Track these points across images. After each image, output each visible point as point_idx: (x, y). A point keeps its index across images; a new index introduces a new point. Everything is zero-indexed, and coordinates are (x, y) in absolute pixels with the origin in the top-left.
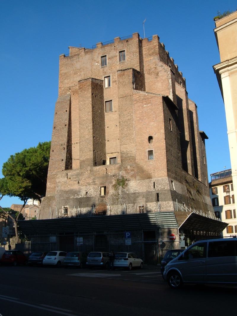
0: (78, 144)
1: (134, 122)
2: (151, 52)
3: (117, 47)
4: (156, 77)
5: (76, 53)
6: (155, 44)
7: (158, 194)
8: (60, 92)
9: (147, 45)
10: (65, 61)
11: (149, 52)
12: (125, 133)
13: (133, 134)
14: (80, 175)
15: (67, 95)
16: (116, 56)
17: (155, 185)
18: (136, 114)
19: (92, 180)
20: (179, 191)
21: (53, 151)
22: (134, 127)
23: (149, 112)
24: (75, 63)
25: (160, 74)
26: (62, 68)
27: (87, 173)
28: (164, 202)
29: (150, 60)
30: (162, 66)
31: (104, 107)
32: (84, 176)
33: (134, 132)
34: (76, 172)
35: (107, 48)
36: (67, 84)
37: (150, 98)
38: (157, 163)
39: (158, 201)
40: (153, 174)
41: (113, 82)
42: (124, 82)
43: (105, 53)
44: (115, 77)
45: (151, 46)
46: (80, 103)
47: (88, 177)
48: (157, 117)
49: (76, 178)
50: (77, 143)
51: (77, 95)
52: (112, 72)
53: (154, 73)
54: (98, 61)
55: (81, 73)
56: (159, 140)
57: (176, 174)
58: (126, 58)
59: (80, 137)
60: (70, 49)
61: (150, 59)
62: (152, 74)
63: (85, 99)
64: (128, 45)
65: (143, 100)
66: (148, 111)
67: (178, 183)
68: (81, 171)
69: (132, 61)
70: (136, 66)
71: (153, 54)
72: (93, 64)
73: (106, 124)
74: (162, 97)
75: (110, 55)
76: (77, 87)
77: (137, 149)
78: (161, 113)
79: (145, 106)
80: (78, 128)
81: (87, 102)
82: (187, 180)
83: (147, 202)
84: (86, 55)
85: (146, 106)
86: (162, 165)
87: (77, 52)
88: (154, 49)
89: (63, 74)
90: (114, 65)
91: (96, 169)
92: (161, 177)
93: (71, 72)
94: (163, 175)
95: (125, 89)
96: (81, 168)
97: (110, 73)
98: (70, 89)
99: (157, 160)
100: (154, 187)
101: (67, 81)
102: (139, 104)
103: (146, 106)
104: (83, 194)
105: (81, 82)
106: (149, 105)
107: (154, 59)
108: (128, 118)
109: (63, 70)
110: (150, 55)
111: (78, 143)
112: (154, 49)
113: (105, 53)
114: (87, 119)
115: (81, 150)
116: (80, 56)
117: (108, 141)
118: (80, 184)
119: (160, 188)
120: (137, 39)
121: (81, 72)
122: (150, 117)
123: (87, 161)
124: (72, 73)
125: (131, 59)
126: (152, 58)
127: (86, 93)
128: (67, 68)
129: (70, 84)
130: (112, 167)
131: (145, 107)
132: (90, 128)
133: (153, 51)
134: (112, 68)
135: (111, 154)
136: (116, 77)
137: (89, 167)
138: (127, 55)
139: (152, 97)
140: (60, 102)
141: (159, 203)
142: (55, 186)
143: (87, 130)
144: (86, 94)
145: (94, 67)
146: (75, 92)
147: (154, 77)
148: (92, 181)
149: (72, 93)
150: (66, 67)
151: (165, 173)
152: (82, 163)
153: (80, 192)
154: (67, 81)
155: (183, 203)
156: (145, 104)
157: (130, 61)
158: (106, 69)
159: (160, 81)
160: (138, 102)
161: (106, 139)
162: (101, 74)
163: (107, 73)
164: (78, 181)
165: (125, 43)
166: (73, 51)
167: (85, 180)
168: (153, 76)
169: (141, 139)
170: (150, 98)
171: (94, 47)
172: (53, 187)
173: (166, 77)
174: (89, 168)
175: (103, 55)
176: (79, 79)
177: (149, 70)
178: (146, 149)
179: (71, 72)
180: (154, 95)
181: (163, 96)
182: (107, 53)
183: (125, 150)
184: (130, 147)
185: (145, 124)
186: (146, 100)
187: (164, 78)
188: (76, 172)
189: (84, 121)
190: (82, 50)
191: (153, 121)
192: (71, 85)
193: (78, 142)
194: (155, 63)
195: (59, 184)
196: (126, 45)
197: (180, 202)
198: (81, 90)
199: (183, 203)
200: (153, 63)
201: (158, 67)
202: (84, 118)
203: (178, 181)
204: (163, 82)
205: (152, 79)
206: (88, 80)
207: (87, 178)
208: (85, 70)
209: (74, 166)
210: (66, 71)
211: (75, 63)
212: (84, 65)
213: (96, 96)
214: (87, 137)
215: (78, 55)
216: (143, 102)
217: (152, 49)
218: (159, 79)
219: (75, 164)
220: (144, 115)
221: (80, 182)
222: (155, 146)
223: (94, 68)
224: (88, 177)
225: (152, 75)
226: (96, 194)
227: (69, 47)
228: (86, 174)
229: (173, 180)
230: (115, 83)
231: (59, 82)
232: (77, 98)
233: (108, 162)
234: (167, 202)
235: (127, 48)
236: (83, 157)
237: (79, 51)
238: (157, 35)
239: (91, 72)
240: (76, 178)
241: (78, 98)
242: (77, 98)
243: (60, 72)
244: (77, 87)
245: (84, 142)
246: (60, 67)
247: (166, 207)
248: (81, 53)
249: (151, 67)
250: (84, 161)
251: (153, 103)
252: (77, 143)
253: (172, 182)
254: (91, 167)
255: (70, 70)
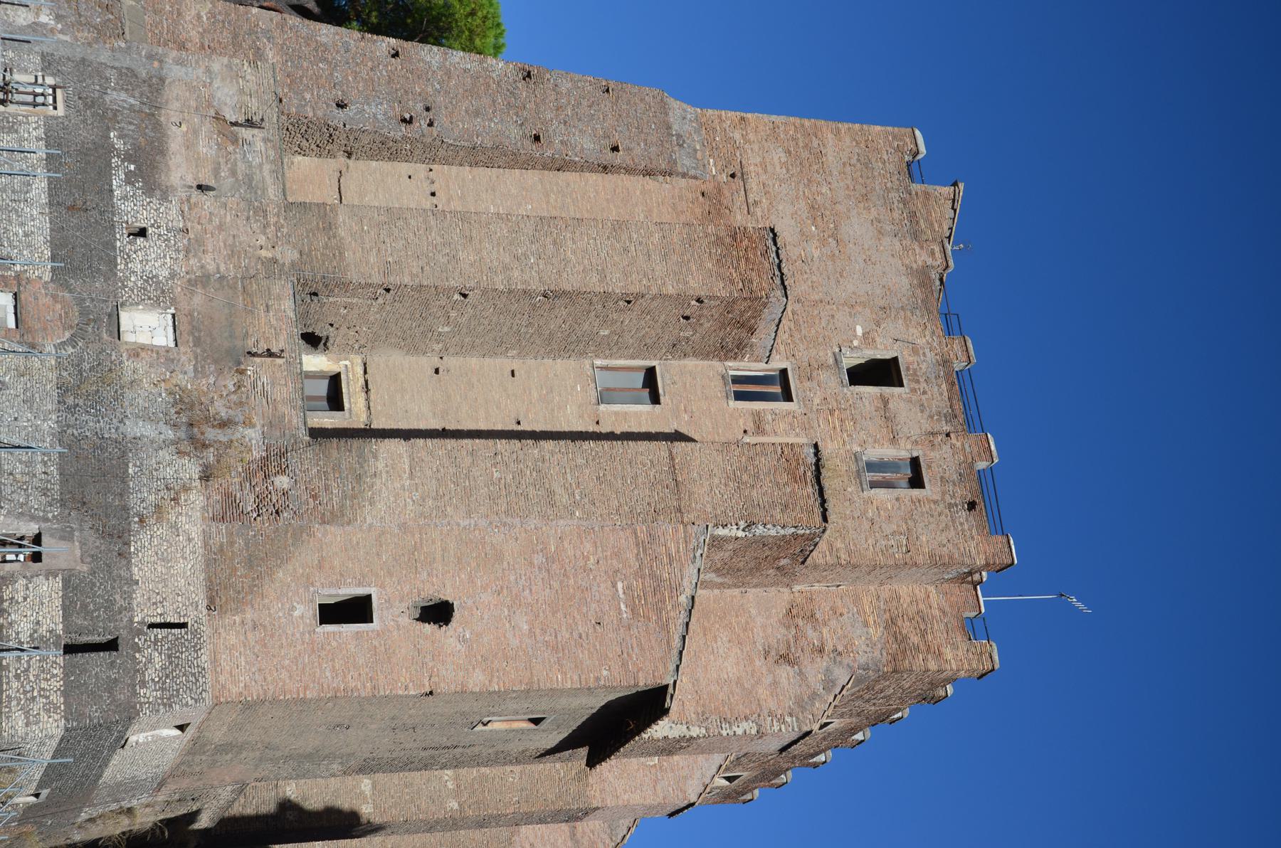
0: (428, 203)
1: (533, 522)
2: (906, 627)
3: (946, 448)
4: (773, 653)
5: (925, 221)
6: (948, 653)
7: (112, 646)
8: (720, 117)
9: (947, 609)
10: (885, 157)
11: (910, 620)
12: (476, 472)
13: (469, 514)
14: (249, 202)
15: (699, 155)
16: (894, 440)
17: (165, 631)
18: (579, 536)
19: (218, 268)
20: (118, 768)
21: (396, 55)
22: (509, 520)
23: (584, 610)
24: (874, 212)
25: (785, 672)
26: (848, 139)
27: (262, 240)
28: (57, 684)
29: (866, 624)
30: (829, 683)
31: (626, 358)
32: (241, 222)
33: (483, 523)
34: (269, 180)
35: (941, 394)
36: (759, 160)
37: (660, 618)
38: (299, 647)
39: (70, 649)
40: (237, 619)
41: (758, 420)
42: (756, 476)
43: (918, 382)
44: (782, 426)
45: (938, 635)
46: (652, 228)
47: (233, 246)
48: (555, 649)
49: (233, 173)
50: (433, 194)
51: (698, 211)
52: (813, 416)
53: (796, 639)
54: (874, 340)
55: (816, 243)
56: (429, 657)
57: (223, 748)
58: (881, 493)
59: (464, 217)
60: (947, 190)
61: (871, 620)
62: (788, 628)
63: (675, 258)
64: (950, 506)
65: (653, 575)
66: (594, 605)
67: (169, 759)
68: (272, 209)
69: (866, 525)
70: (839, 544)
71: (900, 639)
72: (860, 309)
73: (531, 362)
74: (664, 683)
75: (902, 405)
76: (739, 217)
77: (383, 533)
78: (576, 678)
79: (620, 585)
80: (520, 205)
81: (660, 269)
82: (153, 620)
83: (66, 583)
84: (910, 271)
85: (621, 591)
86: (284, 675)
87: (932, 224)
88: (922, 647)
89: (815, 143)
90: (849, 425)
91: (279, 298)
92: (215, 661)
93: (824, 190)
94: (222, 679)
95: (716, 481)
96: (289, 206)
97: (806, 401)
98: (733, 176)
99: (313, 642)
100: (152, 626)
101: (776, 159)
102: (630, 556)
103: (621, 591)
104: (131, 206)
105: (770, 242)
106: (623, 606)
107: (870, 644)
108: (559, 490)
109: (838, 142)
110: (893, 621)
111: (434, 200)
112: (922, 647)
113: (918, 382)
114: (566, 261)
115: (393, 215)
116: (907, 242)
117: (437, 371)
118: (196, 194)
119: (150, 661)
120: (982, 557)
121: (823, 242)
122: (559, 615)
123: (326, 247)
124: (820, 193)
125: (876, 519)
126: (876, 633)
127: (710, 265)
128: (848, 169)
129: (763, 177)
130: (284, 391)
131: (614, 585)
132: (516, 274)
133: (915, 639)
134: (832, 412)
135: (362, 381)
136: (782, 435)
137: (296, 255)
138: (897, 499)
139: (665, 627)
140: (666, 114)
141: (57, 657)
142: (189, 45)
143: (507, 260)
144: (701, 266)
145: (842, 317)
146: (714, 203)
147: (774, 643)
148: (211, 267)
149: (708, 188)
150: (854, 161)
151: (235, 690)
152: (319, 217)
153: (150, 190)
154: (776, 159)
155: (45, 793)
156: (628, 588)
157: (866, 512)
158: (834, 384)
159: (749, 669)
160: (645, 551)
161: (451, 362)
162: (804, 354)
163: (807, 384)
164: (212, 183)
165: (963, 493)
166: (940, 204)
167: (221, 227)
168: (779, 635)
169: (438, 557)
170: (660, 618)
171: (951, 324)
172: (184, 36)
173: (772, 704)
174: (288, 255)
175: (929, 467)
176: (787, 234)
177: (808, 614)
178: (382, 586)
179: (824, 190)
180: (676, 643)
181: (670, 690)
182: (914, 390)
183: (381, 465)
184: (397, 496)
185: (522, 582)
186: (653, 592)
187: (763, 692)
188: (269, 180)
189: (555, 243)
190: (938, 255)
191: (538, 631)
192: (753, 184)
193: (441, 200)
194: (849, 647)
195: (200, 71)
196: (953, 496)
197: (51, 774)
198: (728, 240)
199: (45, 793)
200: (845, 637)
201: (822, 663)
202: (570, 243)
203: (182, 763)
204: (744, 689)
205: (764, 627)
206: (778, 281)
207: (230, 241)
208: (829, 263)
209: (302, 165)
210: (830, 158)
211: (874, 212)
212: (861, 261)
213: (687, 318)
214: (467, 256)
215: (915, 236)
216: (643, 577)
217: (923, 634)
218: (758, 663)
219: (311, 175)
220: (572, 582)
221: (206, 200)
222: (395, 633)
223: (838, 316)
224: (233, 246)
225: (783, 631)
226: (130, 284)
227: (961, 186)
228: (258, 242)
229: (190, 731)
230: (750, 426)
231: (773, 118)
232: (682, 212)
233: (315, 362)
234: (57, 699)
235: (935, 502)
236: (356, 228)
237: (934, 240)
238: (997, 667)
239: (817, 298)
240: (233, 173)
241: (683, 218)
242: (682, 212)
243: (832, 125)
244: (739, 219)
245: (439, 240)
246: (857, 126)
247: (25, 693)
248: (922, 248)
249: (825, 624)
250: (329, 227)
251: (634, 631)
252: (433, 194)
253: (181, 728)
254: (293, 264)
255: (834, 185)
